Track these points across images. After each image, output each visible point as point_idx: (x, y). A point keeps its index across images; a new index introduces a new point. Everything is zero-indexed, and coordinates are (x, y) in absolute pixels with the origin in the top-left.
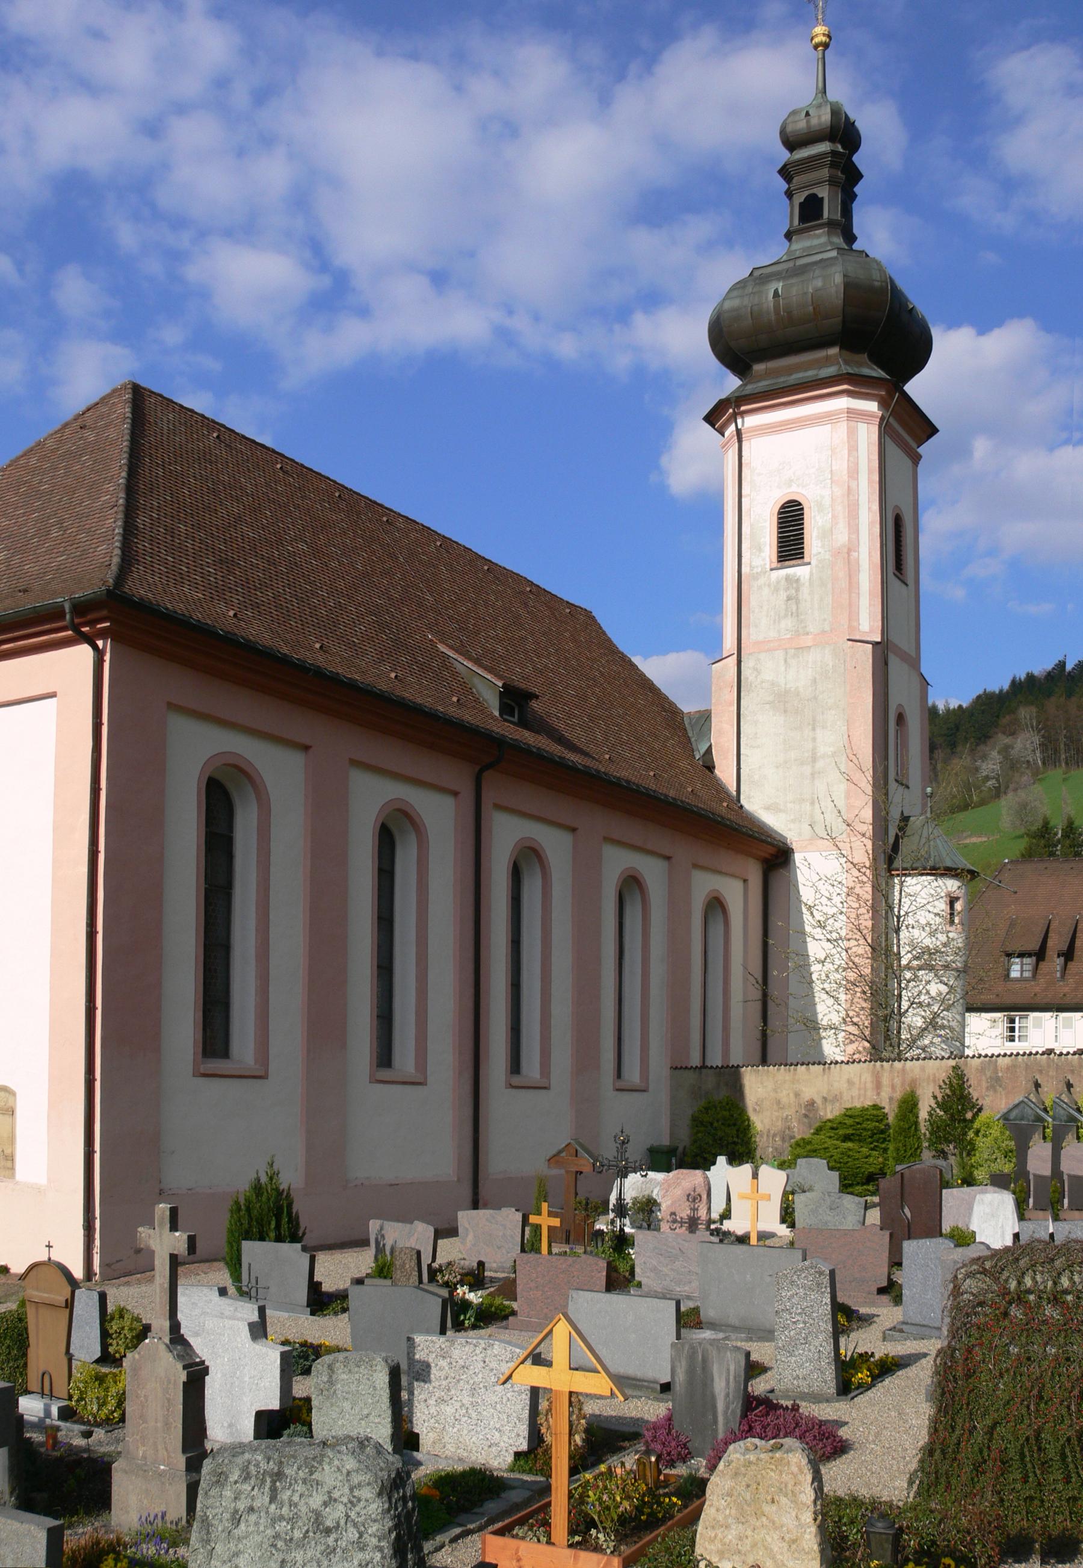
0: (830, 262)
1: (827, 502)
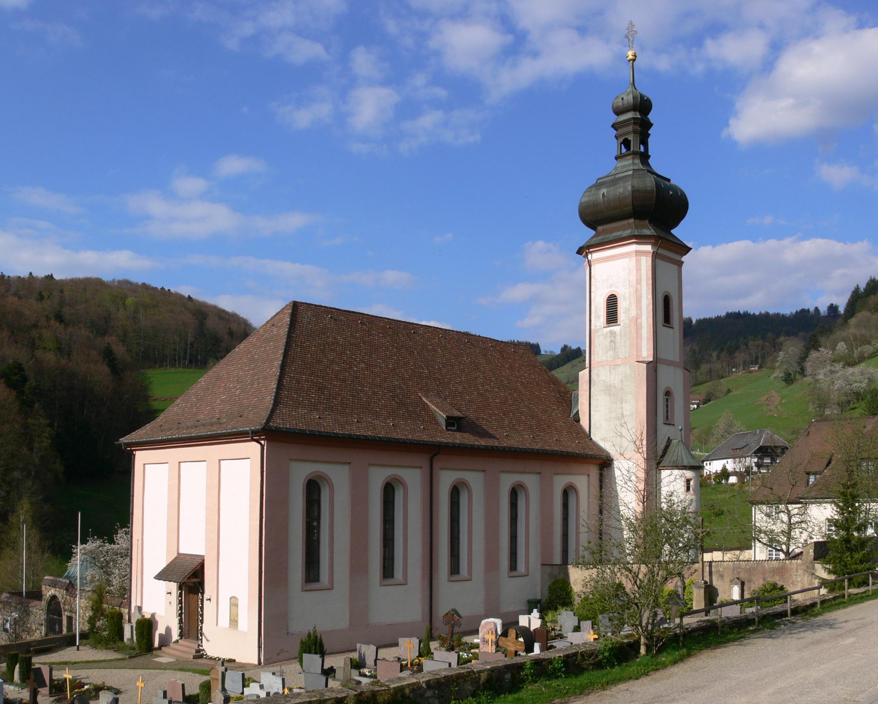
1: (627, 295)
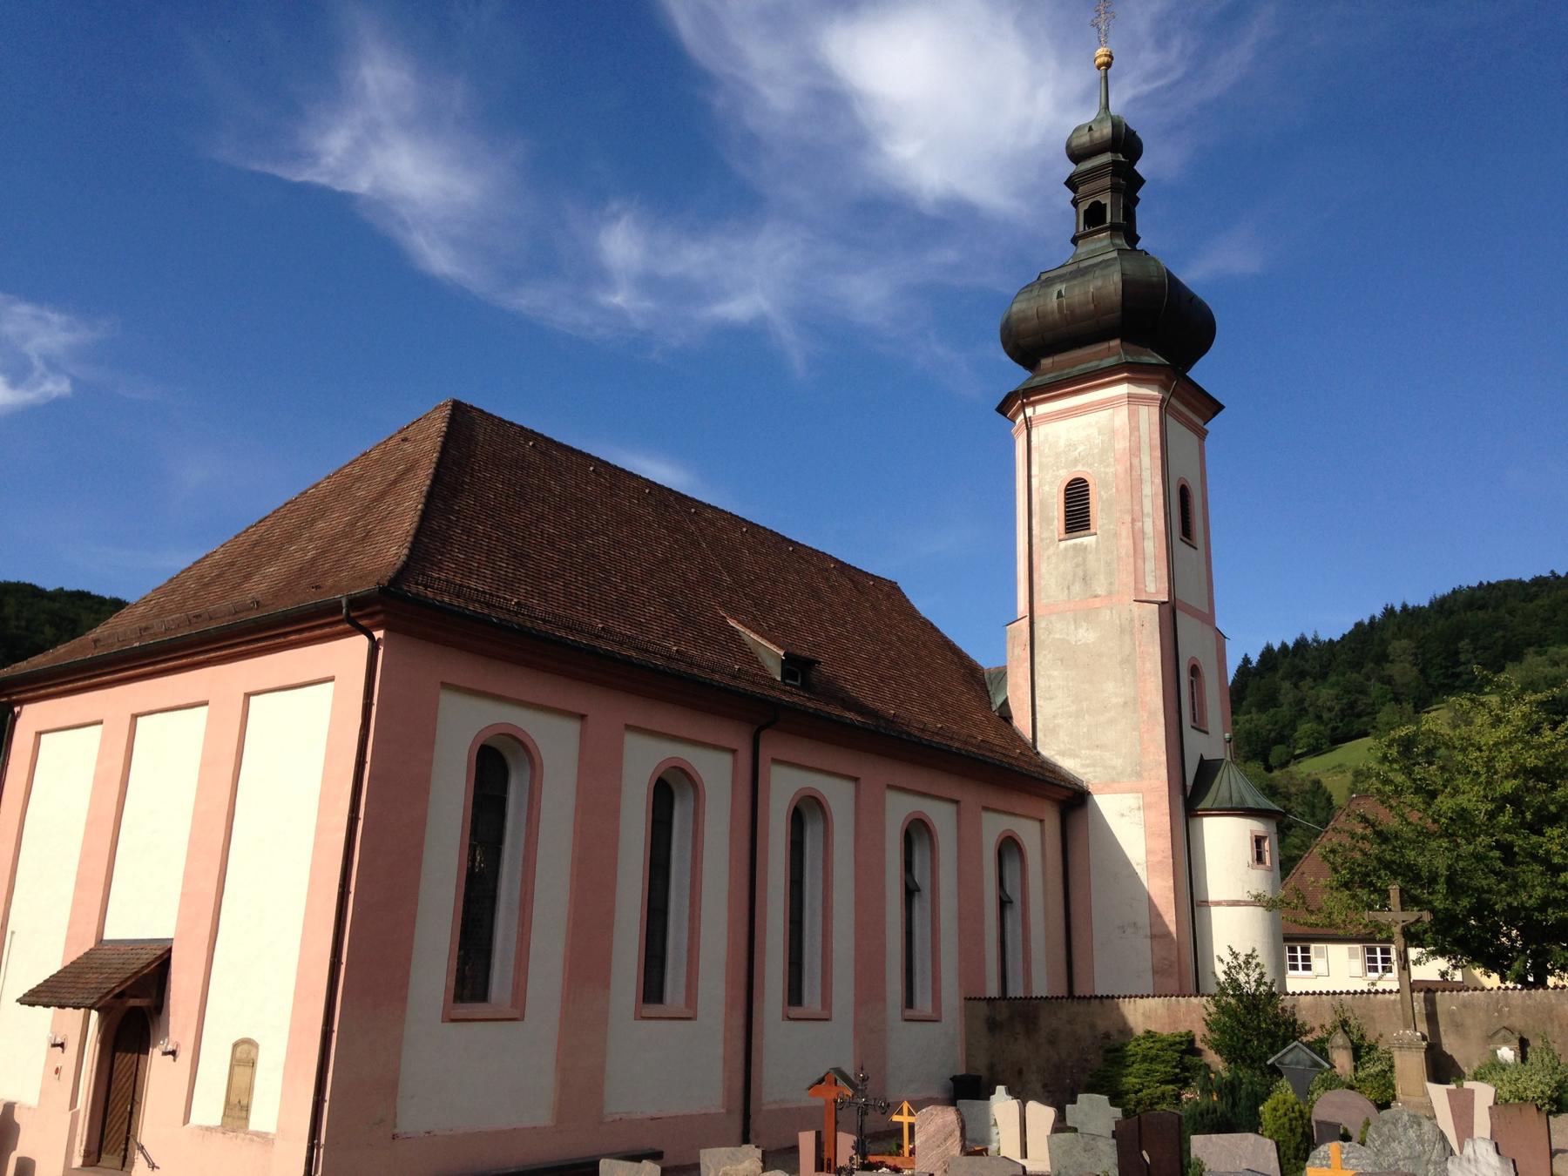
0: (1106, 264)
